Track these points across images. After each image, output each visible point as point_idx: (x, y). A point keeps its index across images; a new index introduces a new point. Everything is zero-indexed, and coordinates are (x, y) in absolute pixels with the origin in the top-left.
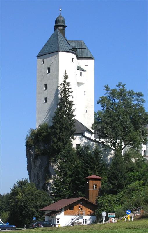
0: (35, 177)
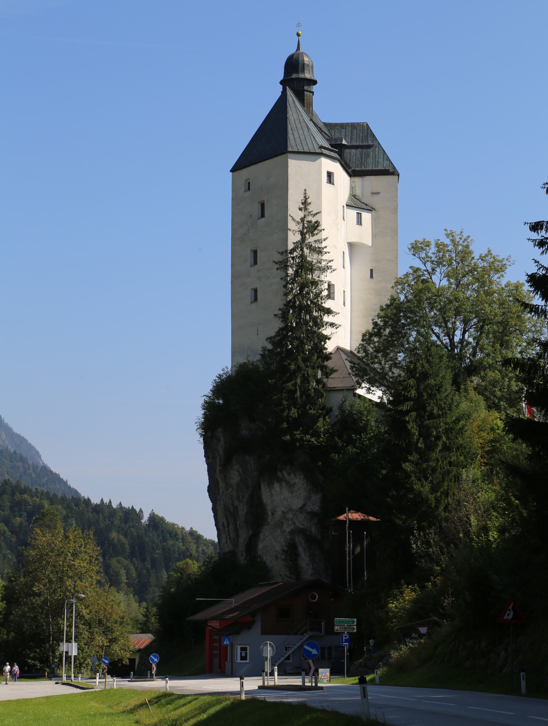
0: (227, 519)
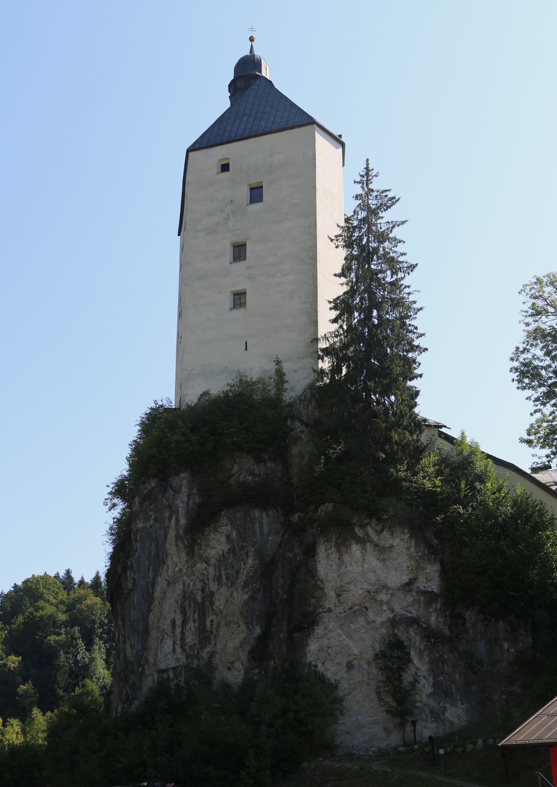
0: (184, 612)
